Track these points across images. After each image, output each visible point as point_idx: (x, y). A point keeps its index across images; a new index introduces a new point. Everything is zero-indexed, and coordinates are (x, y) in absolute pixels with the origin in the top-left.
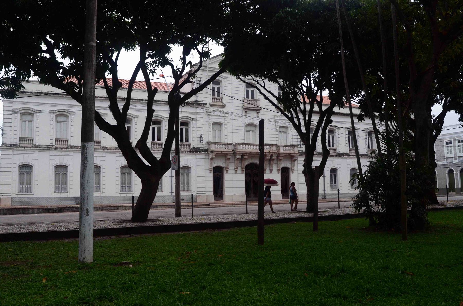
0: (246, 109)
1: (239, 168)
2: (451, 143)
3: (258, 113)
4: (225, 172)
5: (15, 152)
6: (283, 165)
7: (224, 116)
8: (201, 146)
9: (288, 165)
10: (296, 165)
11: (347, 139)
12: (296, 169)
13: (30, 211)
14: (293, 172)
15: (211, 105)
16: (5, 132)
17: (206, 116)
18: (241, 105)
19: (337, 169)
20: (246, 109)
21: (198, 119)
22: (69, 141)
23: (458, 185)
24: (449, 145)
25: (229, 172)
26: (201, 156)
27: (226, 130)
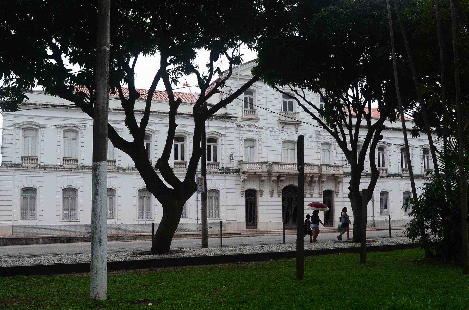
0: (283, 123)
1: (275, 191)
3: (297, 128)
4: (259, 195)
5: (17, 173)
6: (326, 187)
7: (257, 132)
8: (231, 166)
10: (340, 188)
11: (400, 158)
12: (340, 192)
13: (35, 241)
14: (337, 195)
15: (243, 119)
16: (5, 150)
17: (237, 131)
18: (278, 118)
20: (283, 123)
21: (227, 134)
26: (231, 177)
27: (260, 148)
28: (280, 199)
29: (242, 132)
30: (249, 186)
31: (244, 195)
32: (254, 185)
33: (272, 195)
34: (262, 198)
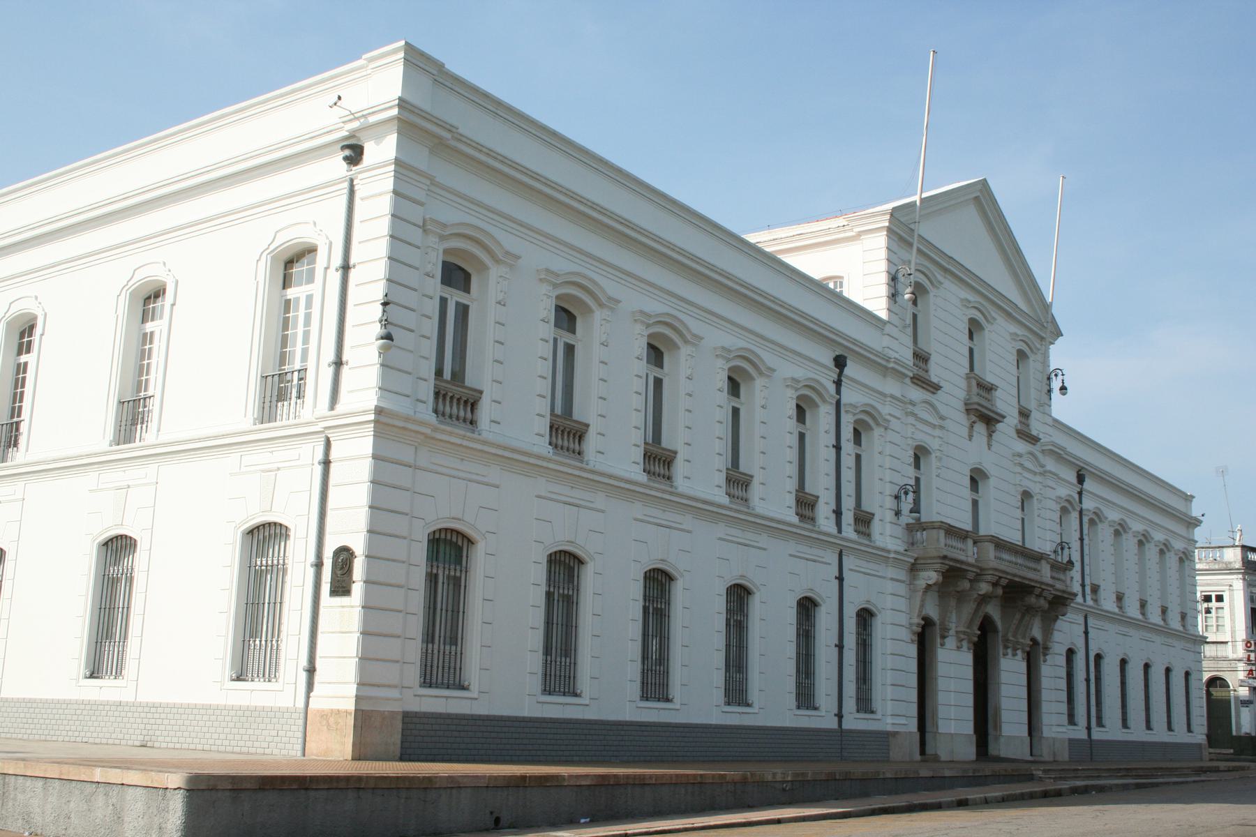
2: (1220, 598)
7: (934, 426)
14: (943, 637)
22: (755, 484)
24: (1214, 604)
29: (911, 420)
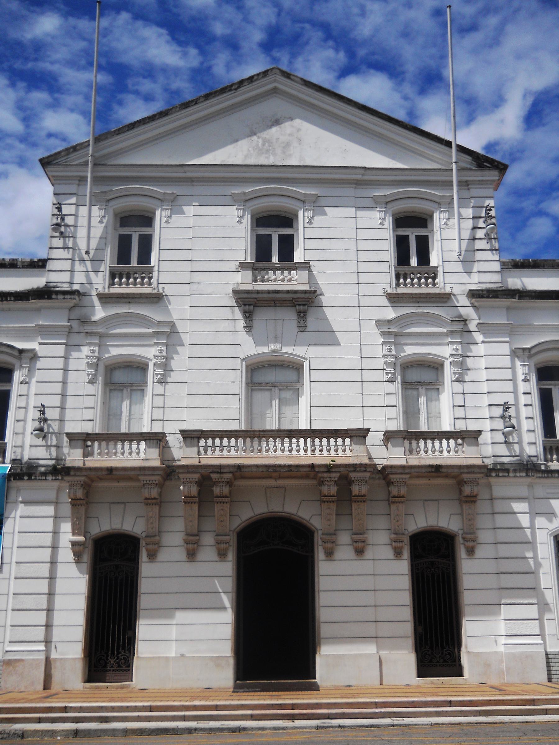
1: (208, 539)
4: (462, 553)
6: (420, 520)
9: (446, 519)
10: (483, 521)
12: (484, 536)
14: (471, 552)
15: (105, 299)
19: (456, 535)
23: (533, 375)
25: (162, 555)
28: (228, 568)
30: (107, 522)
31: (406, 554)
32: (129, 521)
33: (191, 555)
34: (152, 565)
